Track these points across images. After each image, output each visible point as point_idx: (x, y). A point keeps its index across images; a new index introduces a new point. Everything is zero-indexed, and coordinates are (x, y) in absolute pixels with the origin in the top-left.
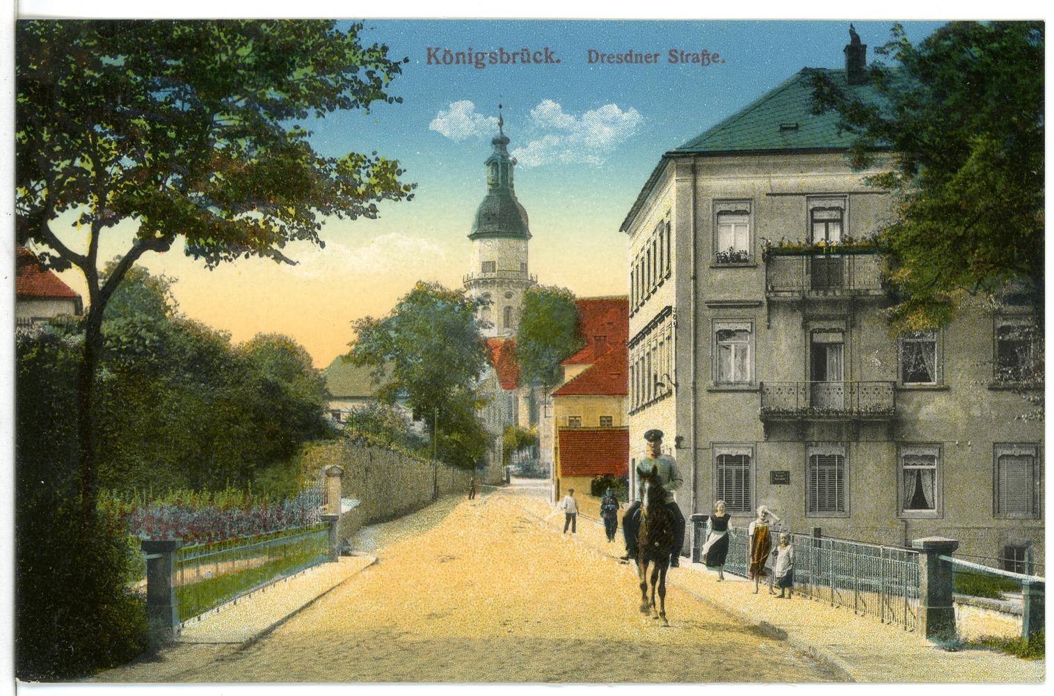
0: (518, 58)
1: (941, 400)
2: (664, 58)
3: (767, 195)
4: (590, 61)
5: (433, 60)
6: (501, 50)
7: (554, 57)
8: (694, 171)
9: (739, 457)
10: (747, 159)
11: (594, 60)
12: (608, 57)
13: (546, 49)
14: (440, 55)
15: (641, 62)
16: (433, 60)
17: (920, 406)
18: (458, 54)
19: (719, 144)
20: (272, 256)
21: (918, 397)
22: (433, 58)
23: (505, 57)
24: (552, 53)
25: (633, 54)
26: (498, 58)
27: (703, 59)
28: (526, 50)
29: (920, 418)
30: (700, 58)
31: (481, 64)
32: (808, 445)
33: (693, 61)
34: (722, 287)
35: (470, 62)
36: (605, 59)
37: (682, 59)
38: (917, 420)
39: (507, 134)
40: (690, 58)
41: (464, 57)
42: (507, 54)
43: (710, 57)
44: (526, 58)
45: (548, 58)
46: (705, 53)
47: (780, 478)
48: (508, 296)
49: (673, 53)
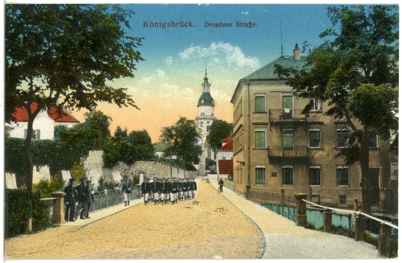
0: (179, 24)
1: (321, 152)
2: (234, 24)
3: (270, 92)
4: (206, 26)
5: (146, 25)
6: (172, 22)
7: (193, 25)
8: (249, 85)
9: (262, 168)
10: (263, 82)
11: (207, 26)
12: (213, 25)
13: (189, 21)
14: (148, 24)
15: (225, 26)
16: (146, 25)
17: (315, 154)
18: (155, 24)
19: (256, 77)
20: (20, 92)
21: (314, 152)
22: (145, 25)
23: (174, 24)
24: (192, 23)
25: (222, 24)
26: (171, 24)
27: (249, 26)
28: (182, 22)
29: (315, 157)
30: (248, 25)
31: (165, 27)
32: (283, 165)
33: (246, 26)
34: (256, 118)
35: (160, 26)
36: (211, 25)
37: (241, 25)
38: (314, 158)
39: (208, 77)
40: (244, 25)
41: (158, 24)
42: (174, 23)
43: (252, 25)
44: (182, 25)
45: (190, 25)
46: (250, 23)
47: (274, 175)
48: (208, 123)
49: (238, 23)
